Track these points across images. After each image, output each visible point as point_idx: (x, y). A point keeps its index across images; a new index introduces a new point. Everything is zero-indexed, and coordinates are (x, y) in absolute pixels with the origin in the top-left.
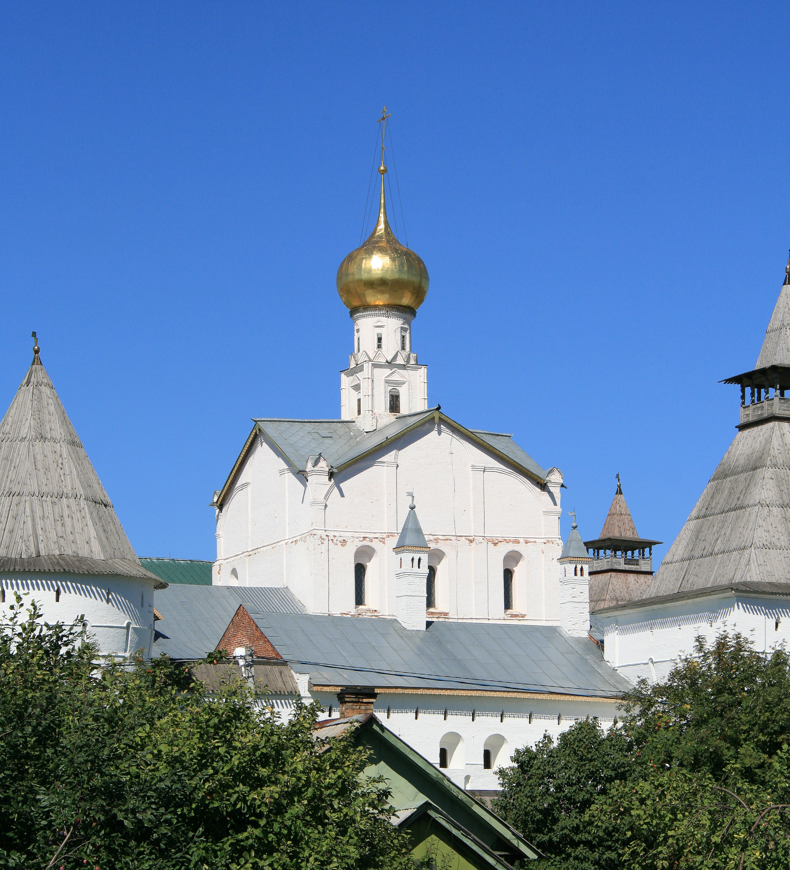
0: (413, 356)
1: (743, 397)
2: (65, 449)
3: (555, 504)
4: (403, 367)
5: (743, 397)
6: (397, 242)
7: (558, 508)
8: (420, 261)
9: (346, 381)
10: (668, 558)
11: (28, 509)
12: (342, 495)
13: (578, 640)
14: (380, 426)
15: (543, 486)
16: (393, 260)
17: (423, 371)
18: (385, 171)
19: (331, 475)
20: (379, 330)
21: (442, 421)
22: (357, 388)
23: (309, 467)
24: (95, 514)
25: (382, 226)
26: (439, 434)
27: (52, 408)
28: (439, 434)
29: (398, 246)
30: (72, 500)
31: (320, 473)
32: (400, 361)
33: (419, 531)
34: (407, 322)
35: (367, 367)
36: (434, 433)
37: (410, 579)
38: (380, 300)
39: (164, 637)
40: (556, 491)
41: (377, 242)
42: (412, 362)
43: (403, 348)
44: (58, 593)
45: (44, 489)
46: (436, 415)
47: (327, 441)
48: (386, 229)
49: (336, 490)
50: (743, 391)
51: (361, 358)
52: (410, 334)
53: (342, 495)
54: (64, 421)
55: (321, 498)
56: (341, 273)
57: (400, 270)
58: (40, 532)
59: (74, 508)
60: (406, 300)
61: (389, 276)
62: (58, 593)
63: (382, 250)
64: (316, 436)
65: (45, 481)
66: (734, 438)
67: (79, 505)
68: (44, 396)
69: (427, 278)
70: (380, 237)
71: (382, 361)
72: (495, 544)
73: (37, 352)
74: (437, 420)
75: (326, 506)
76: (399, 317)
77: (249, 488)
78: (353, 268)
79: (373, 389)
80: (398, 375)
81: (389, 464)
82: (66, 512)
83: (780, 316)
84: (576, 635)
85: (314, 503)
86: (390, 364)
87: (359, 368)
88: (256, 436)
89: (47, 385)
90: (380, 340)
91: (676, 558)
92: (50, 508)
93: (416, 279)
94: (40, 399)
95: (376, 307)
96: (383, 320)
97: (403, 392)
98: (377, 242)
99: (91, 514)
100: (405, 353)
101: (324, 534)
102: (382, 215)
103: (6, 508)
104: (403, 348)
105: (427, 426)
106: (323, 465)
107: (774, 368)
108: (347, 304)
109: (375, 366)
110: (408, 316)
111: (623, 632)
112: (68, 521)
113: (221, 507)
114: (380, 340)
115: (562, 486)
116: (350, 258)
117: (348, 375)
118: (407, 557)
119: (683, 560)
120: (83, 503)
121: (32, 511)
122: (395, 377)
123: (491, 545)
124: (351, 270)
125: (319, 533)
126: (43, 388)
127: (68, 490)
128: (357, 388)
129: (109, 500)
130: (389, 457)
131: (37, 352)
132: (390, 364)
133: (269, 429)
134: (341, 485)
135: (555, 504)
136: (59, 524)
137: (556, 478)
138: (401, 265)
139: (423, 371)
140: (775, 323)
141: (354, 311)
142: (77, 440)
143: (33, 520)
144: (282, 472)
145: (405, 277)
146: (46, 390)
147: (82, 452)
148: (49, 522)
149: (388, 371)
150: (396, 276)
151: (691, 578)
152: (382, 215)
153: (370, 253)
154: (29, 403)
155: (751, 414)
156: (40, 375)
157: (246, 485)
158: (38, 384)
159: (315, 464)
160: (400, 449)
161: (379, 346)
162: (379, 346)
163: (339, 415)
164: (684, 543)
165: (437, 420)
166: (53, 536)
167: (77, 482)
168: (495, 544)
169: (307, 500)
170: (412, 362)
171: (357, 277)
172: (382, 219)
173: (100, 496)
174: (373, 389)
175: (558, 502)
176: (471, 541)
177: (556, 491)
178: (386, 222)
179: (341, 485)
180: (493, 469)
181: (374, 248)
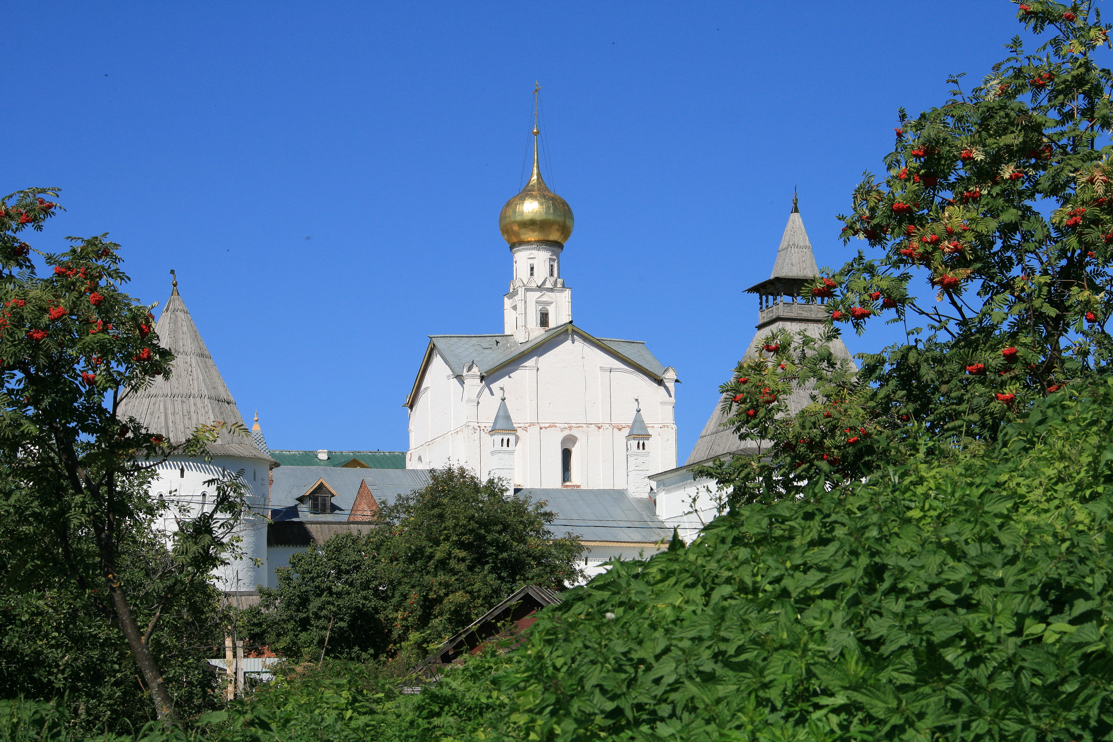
0: (560, 281)
1: (761, 303)
2: (194, 360)
3: (670, 396)
4: (551, 290)
5: (761, 303)
6: (547, 189)
7: (673, 400)
8: (565, 204)
9: (508, 303)
10: (703, 434)
11: (162, 407)
12: (492, 394)
13: (640, 501)
14: (531, 338)
15: (660, 382)
16: (541, 204)
17: (568, 293)
18: (538, 133)
19: (482, 378)
20: (531, 261)
21: (574, 332)
22: (515, 308)
23: (465, 373)
24: (217, 410)
25: (535, 177)
26: (573, 342)
27: (185, 329)
28: (573, 342)
29: (546, 193)
30: (198, 399)
31: (473, 376)
32: (548, 285)
33: (508, 418)
34: (554, 253)
35: (521, 291)
36: (569, 342)
37: (500, 455)
38: (532, 236)
39: (340, 509)
40: (671, 385)
41: (530, 191)
42: (559, 286)
43: (552, 275)
44: (182, 471)
45: (176, 391)
46: (570, 327)
47: (487, 351)
48: (538, 179)
49: (487, 390)
50: (761, 298)
51: (518, 283)
52: (558, 263)
53: (492, 394)
54: (195, 338)
55: (474, 397)
56: (502, 217)
57: (547, 213)
58: (170, 424)
59: (199, 405)
60: (555, 236)
61: (538, 218)
62: (182, 471)
63: (533, 197)
64: (478, 348)
65: (176, 385)
66: (754, 336)
67: (204, 403)
68: (179, 319)
69: (572, 218)
70: (533, 186)
71: (534, 285)
72: (620, 429)
73: (175, 285)
74: (570, 331)
75: (478, 403)
76: (547, 250)
77: (429, 391)
78: (509, 212)
79: (525, 308)
80: (547, 297)
81: (531, 368)
82: (193, 409)
83: (787, 238)
84: (638, 496)
85: (469, 401)
86: (540, 288)
87: (515, 293)
88: (432, 350)
89: (182, 311)
90: (532, 269)
91: (709, 432)
92: (180, 407)
93: (560, 219)
94: (175, 322)
95: (529, 243)
96: (535, 253)
97: (551, 311)
98: (530, 191)
99: (213, 410)
100: (553, 279)
101: (476, 425)
102: (535, 169)
103: (146, 407)
104: (552, 275)
105: (562, 336)
106: (475, 370)
107: (777, 279)
108: (508, 241)
109: (527, 290)
110: (555, 249)
111: (668, 492)
112: (194, 416)
113: (411, 407)
114: (532, 269)
115: (677, 381)
116: (508, 204)
117: (509, 298)
118: (498, 438)
119: (712, 434)
120: (207, 401)
121: (165, 409)
122: (545, 299)
123: (616, 430)
124: (508, 214)
125: (472, 424)
126: (179, 313)
127: (195, 391)
128: (515, 308)
129: (232, 399)
130: (531, 362)
131: (175, 285)
132: (540, 288)
133: (440, 343)
134: (491, 386)
135: (670, 396)
136: (186, 418)
137: (670, 376)
138: (548, 208)
139: (568, 293)
140: (783, 244)
141: (512, 246)
142: (206, 353)
143: (166, 416)
144: (448, 377)
145: (551, 217)
146: (181, 315)
147: (210, 362)
148: (178, 418)
149: (539, 294)
150: (544, 217)
151: (715, 447)
152: (535, 169)
153: (523, 199)
154: (167, 325)
155: (762, 317)
156: (177, 303)
157: (427, 389)
158: (175, 310)
159: (470, 369)
160: (540, 356)
161: (532, 274)
162: (532, 274)
163: (503, 331)
164: (714, 420)
165: (570, 331)
166: (181, 427)
167: (203, 385)
168: (620, 429)
169: (464, 399)
170: (559, 286)
171: (513, 219)
172: (535, 171)
173: (224, 395)
174: (525, 308)
175: (673, 394)
176: (599, 428)
177: (671, 385)
178: (539, 174)
179: (491, 386)
180: (617, 370)
181: (527, 195)
